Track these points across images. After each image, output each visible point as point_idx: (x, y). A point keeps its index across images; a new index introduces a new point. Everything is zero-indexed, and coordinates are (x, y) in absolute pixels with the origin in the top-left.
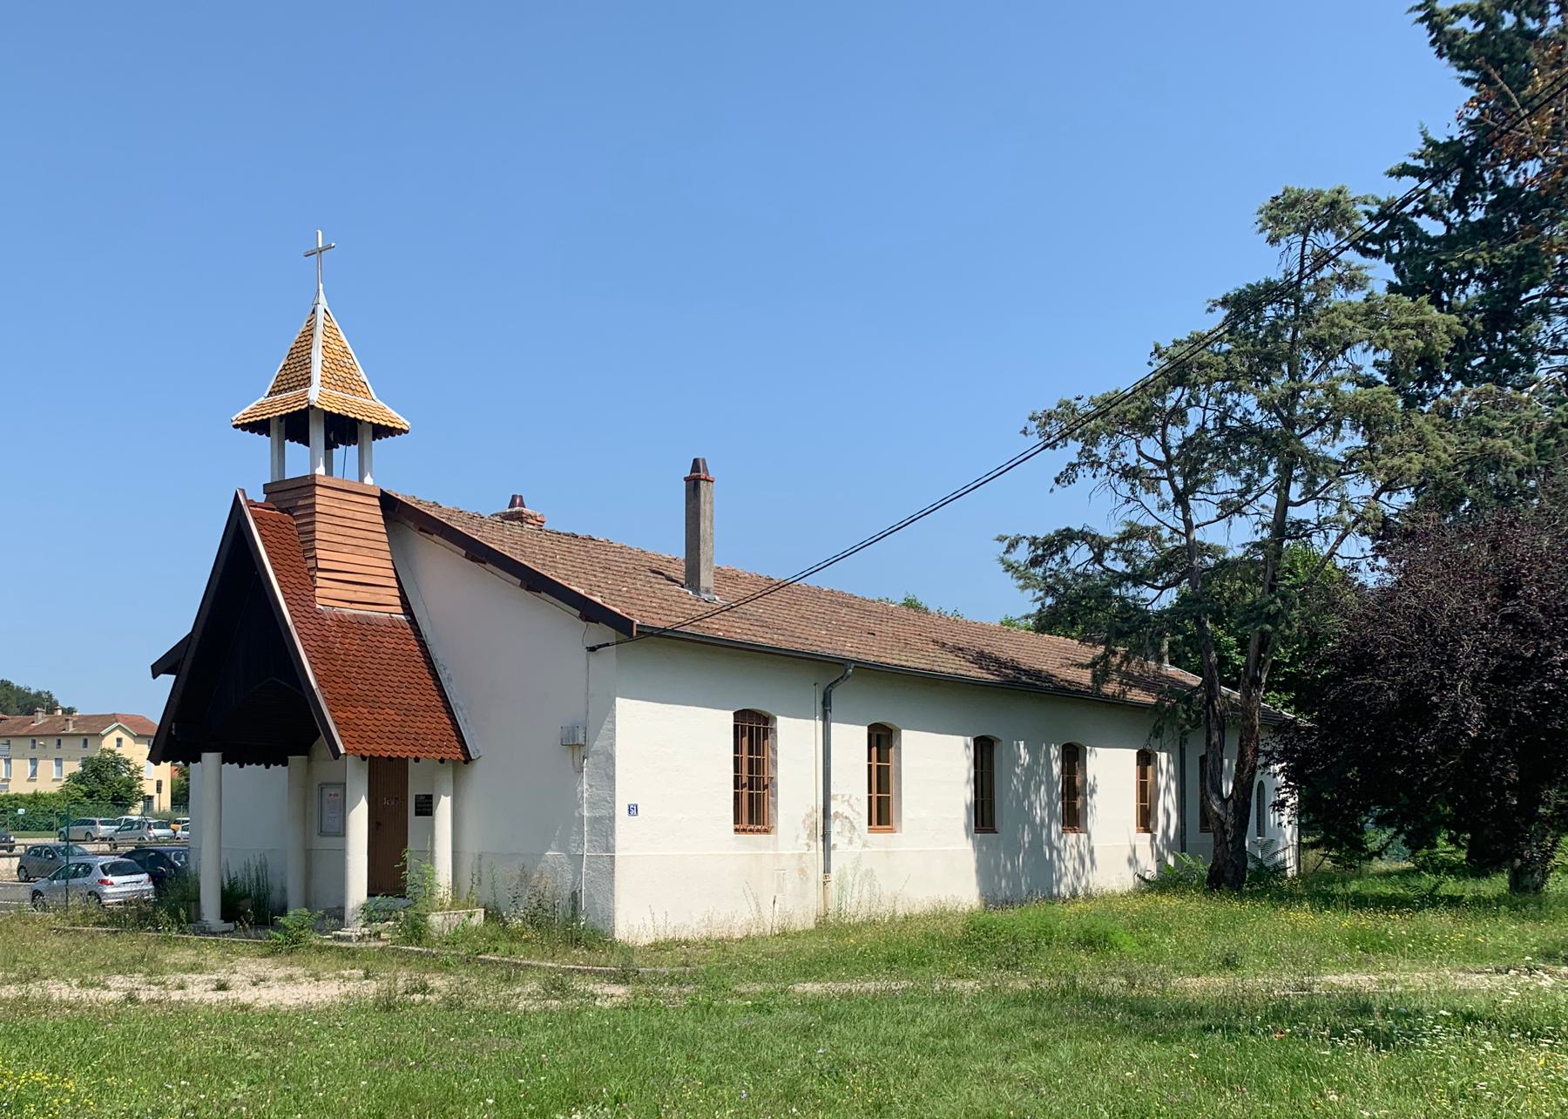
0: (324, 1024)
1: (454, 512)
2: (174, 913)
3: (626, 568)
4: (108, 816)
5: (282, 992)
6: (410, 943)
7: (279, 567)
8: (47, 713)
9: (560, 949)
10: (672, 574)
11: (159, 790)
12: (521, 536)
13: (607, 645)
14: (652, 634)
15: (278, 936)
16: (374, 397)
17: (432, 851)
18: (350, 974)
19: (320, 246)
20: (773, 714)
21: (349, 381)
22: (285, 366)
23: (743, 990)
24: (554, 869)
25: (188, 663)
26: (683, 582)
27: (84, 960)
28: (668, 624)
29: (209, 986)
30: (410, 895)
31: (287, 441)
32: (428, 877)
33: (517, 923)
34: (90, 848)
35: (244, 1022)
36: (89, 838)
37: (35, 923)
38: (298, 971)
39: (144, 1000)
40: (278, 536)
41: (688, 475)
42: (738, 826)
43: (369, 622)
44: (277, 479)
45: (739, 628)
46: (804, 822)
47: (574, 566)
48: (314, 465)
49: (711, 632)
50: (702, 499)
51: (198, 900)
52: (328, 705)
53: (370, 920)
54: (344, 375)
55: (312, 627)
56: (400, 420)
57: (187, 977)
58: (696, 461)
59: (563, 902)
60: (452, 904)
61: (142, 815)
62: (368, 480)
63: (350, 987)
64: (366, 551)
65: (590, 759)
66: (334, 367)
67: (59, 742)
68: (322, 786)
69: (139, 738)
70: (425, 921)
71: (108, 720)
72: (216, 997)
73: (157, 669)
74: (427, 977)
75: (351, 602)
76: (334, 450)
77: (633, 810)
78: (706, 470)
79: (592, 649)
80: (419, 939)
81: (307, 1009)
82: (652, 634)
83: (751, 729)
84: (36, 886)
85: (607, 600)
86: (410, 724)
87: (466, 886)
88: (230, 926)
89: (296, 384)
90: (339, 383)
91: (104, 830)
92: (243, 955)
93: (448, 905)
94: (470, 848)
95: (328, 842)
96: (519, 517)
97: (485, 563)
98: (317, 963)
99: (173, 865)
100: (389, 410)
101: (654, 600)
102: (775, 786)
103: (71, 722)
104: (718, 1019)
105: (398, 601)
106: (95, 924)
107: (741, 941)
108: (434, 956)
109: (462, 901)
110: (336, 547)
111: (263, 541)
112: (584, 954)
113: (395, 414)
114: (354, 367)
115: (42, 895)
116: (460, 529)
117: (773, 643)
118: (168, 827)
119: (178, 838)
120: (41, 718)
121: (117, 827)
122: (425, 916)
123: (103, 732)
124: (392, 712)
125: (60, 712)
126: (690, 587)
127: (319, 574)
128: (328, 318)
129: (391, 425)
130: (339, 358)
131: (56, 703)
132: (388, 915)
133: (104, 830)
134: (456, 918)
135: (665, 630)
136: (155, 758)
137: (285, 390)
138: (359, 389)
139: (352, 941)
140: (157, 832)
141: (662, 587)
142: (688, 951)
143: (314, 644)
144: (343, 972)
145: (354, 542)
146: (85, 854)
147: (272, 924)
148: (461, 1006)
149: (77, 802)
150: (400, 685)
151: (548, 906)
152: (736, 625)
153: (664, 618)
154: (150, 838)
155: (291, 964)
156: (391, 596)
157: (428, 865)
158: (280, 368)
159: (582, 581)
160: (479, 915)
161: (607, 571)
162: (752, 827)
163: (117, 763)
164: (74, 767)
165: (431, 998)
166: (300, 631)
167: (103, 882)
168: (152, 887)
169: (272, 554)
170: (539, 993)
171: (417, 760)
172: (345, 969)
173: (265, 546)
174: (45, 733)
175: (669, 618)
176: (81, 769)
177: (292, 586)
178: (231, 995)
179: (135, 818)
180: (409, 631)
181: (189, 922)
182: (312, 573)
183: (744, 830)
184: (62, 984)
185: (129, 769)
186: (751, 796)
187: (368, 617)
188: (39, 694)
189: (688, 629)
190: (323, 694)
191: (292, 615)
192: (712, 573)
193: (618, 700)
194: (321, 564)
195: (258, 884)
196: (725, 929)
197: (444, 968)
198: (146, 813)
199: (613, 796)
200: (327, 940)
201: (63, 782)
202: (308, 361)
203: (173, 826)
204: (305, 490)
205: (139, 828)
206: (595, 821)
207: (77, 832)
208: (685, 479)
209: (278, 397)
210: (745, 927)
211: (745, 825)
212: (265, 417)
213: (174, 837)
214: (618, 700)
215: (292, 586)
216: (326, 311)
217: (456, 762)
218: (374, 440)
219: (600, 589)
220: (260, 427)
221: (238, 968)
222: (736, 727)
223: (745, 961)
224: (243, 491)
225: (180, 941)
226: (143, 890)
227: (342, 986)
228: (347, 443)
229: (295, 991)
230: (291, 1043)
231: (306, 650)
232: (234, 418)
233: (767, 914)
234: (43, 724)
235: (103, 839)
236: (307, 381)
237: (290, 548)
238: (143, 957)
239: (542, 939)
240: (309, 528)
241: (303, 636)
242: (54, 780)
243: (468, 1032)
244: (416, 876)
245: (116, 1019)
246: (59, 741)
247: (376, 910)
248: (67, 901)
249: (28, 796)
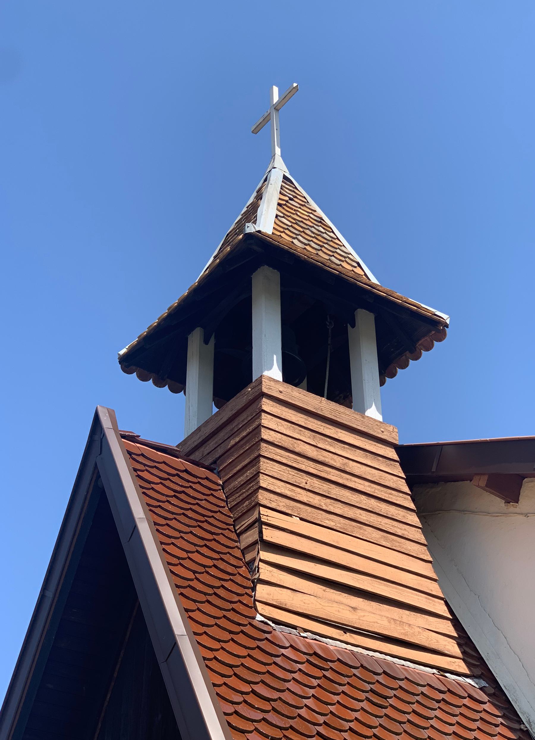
64: (376, 535)
127: (265, 555)
187: (388, 664)
194: (269, 535)
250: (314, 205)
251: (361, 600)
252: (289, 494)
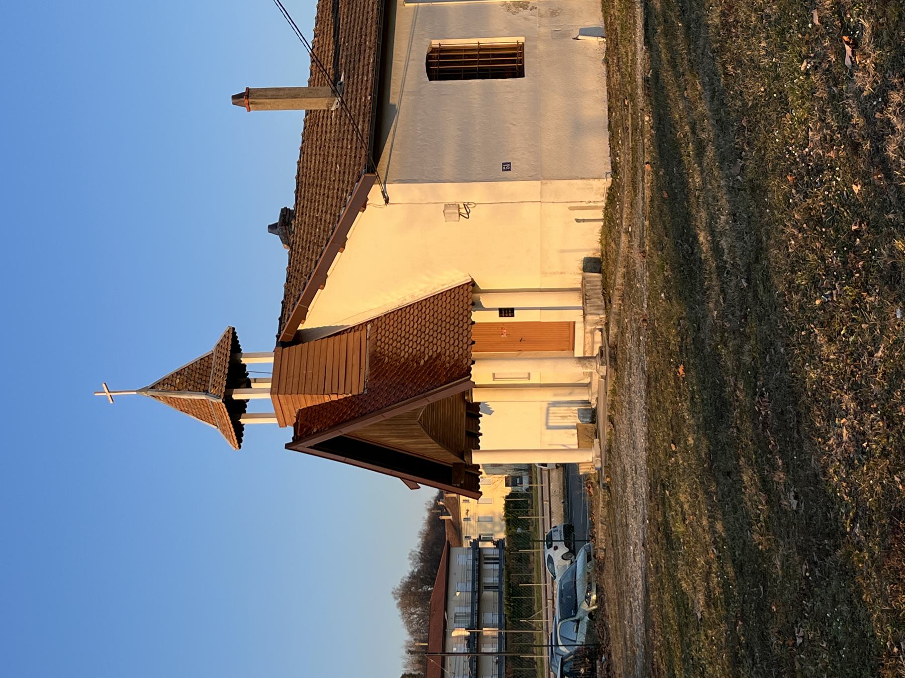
22: (194, 415)
46: (514, 13)
57: (685, 603)
79: (387, 201)
202: (190, 401)
240: (308, 390)
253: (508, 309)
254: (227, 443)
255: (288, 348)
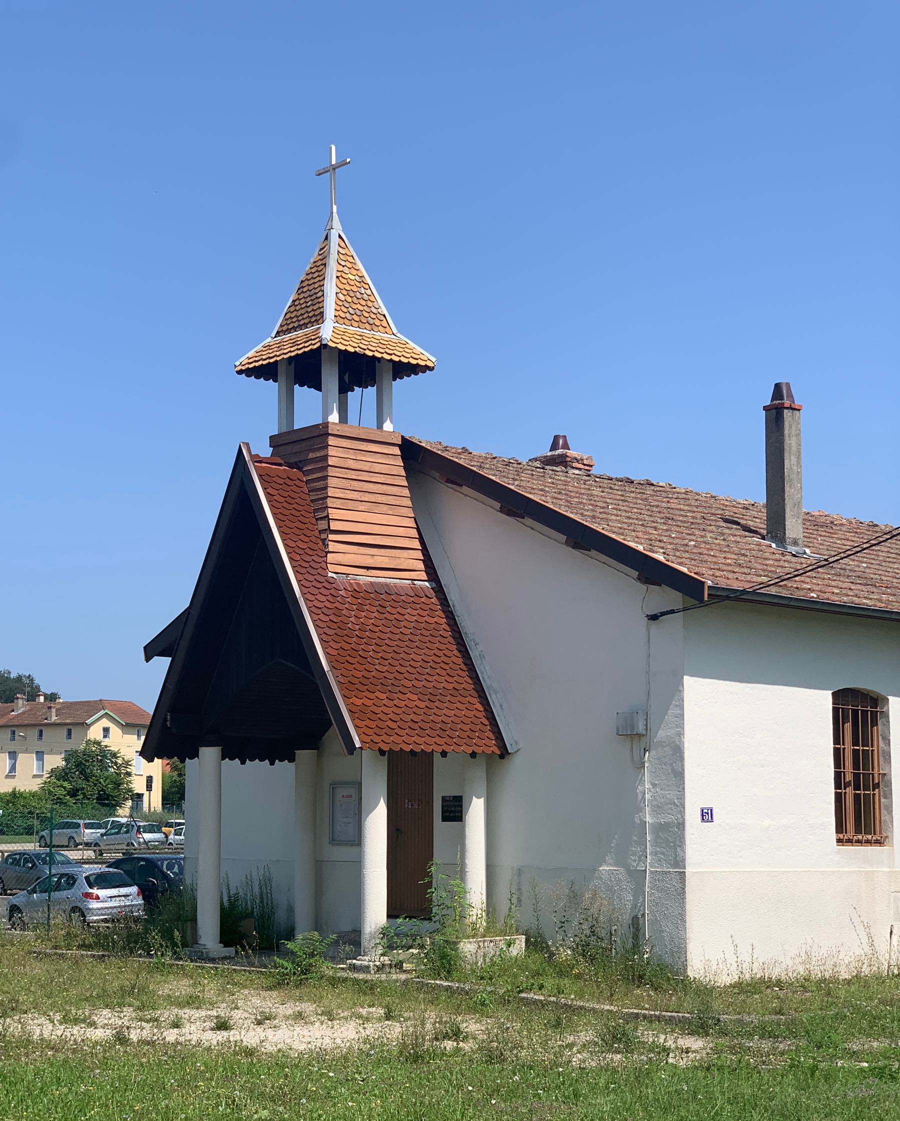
0: (341, 1077)
1: (486, 458)
2: (167, 935)
3: (693, 518)
4: (94, 817)
5: (290, 1033)
6: (438, 976)
7: (287, 530)
8: (28, 701)
9: (620, 988)
10: (750, 523)
11: (149, 787)
12: (566, 483)
13: (672, 612)
14: (728, 597)
15: (285, 964)
16: (395, 331)
17: (463, 865)
18: (369, 1013)
19: (334, 162)
20: (883, 694)
21: (367, 315)
22: (294, 301)
23: (855, 1048)
24: (610, 889)
25: (184, 644)
26: (764, 532)
27: (67, 991)
28: (747, 586)
29: (208, 1024)
30: (437, 918)
31: (297, 387)
32: (458, 895)
33: (565, 954)
34: (73, 855)
35: (249, 1072)
36: (72, 844)
37: (13, 945)
38: (308, 1008)
39: (135, 1040)
40: (286, 494)
41: (768, 403)
42: (841, 836)
43: (388, 590)
44: (284, 430)
45: (837, 587)
47: (629, 518)
48: (326, 412)
49: (802, 593)
50: (786, 432)
51: (194, 920)
52: (341, 690)
53: (391, 947)
54: (361, 308)
55: (323, 598)
56: (424, 356)
57: (186, 1013)
58: (778, 387)
59: (621, 929)
60: (487, 929)
61: (131, 816)
62: (388, 426)
63: (371, 1030)
64: (384, 508)
65: (653, 752)
66: (349, 300)
67: (41, 733)
68: (334, 786)
69: (128, 727)
70: (456, 950)
71: (92, 707)
72: (215, 1038)
73: (151, 651)
74: (460, 1018)
75: (368, 568)
76: (349, 393)
77: (707, 815)
78: (790, 396)
79: (654, 618)
80: (449, 972)
81: (319, 1056)
82: (728, 597)
83: (855, 712)
84: (14, 900)
85: (671, 558)
86: (436, 711)
87: (503, 906)
88: (231, 951)
89: (306, 321)
90: (355, 317)
91: (89, 834)
92: (245, 987)
93: (481, 930)
94: (508, 861)
95: (340, 853)
96: (562, 461)
97: (523, 518)
98: (330, 999)
99: (166, 876)
100: (412, 344)
101: (729, 556)
102: (889, 784)
103: (54, 710)
104: (827, 1087)
105: (421, 566)
106: (80, 947)
107: (848, 982)
108: (467, 993)
109: (498, 926)
110: (351, 505)
111: (269, 501)
112: (649, 996)
113: (418, 349)
114: (372, 298)
115: (20, 912)
116: (493, 478)
117: (880, 605)
118: (160, 831)
119: (170, 844)
120: (21, 705)
121: (103, 831)
122: (455, 943)
123: (88, 721)
124: (415, 697)
125: (42, 699)
126: (774, 538)
127: (332, 537)
128: (342, 244)
129: (414, 362)
130: (355, 289)
131: (38, 688)
132: (411, 940)
133: (89, 834)
134: (493, 946)
135: (744, 592)
136: (148, 753)
137: (295, 329)
138: (377, 322)
139: (370, 972)
140: (147, 836)
141: (738, 539)
142: (781, 994)
143: (326, 619)
144: (361, 1010)
145: (372, 498)
146: (68, 862)
147: (278, 947)
148: (502, 1059)
149: (60, 801)
150: (424, 665)
151: (603, 934)
152: (833, 583)
153: (743, 577)
154: (139, 843)
155: (301, 999)
156: (413, 560)
157: (458, 881)
158: (289, 304)
159: (640, 535)
160: (520, 943)
161: (670, 522)
162: (860, 837)
163: (105, 756)
164: (55, 761)
165: (466, 1046)
166: (310, 604)
167: (88, 896)
168: (141, 902)
169: (279, 516)
170: (596, 1044)
171: (444, 754)
172: (362, 1007)
173: (272, 507)
174: (26, 722)
175: (749, 578)
176: (64, 763)
177: (301, 552)
178: (233, 1035)
179: (124, 820)
180: (434, 600)
181: (185, 945)
182: (323, 536)
183: (849, 841)
184: (42, 1020)
185: (116, 763)
186: (857, 798)
187: (387, 585)
188: (19, 678)
189: (773, 591)
190: (336, 677)
191: (301, 586)
192: (800, 521)
193: (686, 679)
194: (334, 526)
195: (262, 901)
196: (829, 966)
197: (479, 1008)
198: (135, 815)
199: (682, 797)
200: (340, 970)
201: (44, 779)
202: (320, 294)
203: (164, 829)
204: (317, 440)
205: (127, 832)
206: (659, 828)
207: (60, 836)
208: (765, 408)
209: (287, 337)
210: (853, 964)
211: (850, 834)
212: (272, 361)
213: (166, 842)
214: (686, 679)
215: (301, 552)
216: (340, 237)
217: (489, 757)
218: (394, 380)
219: (662, 545)
220: (265, 371)
221: (240, 1003)
222: (835, 711)
223: (857, 1009)
224: (247, 445)
225: (175, 968)
226: (133, 905)
227: (361, 1029)
228: (363, 385)
229: (306, 1033)
230: (304, 1101)
231: (316, 626)
232: (237, 363)
233: (882, 946)
234: (24, 713)
235: (87, 844)
236: (320, 317)
237: (299, 508)
238: (133, 988)
239: (596, 974)
241: (313, 609)
242: (35, 776)
243: (513, 1093)
244: (444, 895)
245: (104, 1064)
246: (41, 732)
247: (397, 935)
248: (49, 919)
249: (5, 794)
250: (360, 266)
251: (376, 549)
252: (342, 496)
253: (151, 787)
254: (248, 356)
255: (400, 454)
